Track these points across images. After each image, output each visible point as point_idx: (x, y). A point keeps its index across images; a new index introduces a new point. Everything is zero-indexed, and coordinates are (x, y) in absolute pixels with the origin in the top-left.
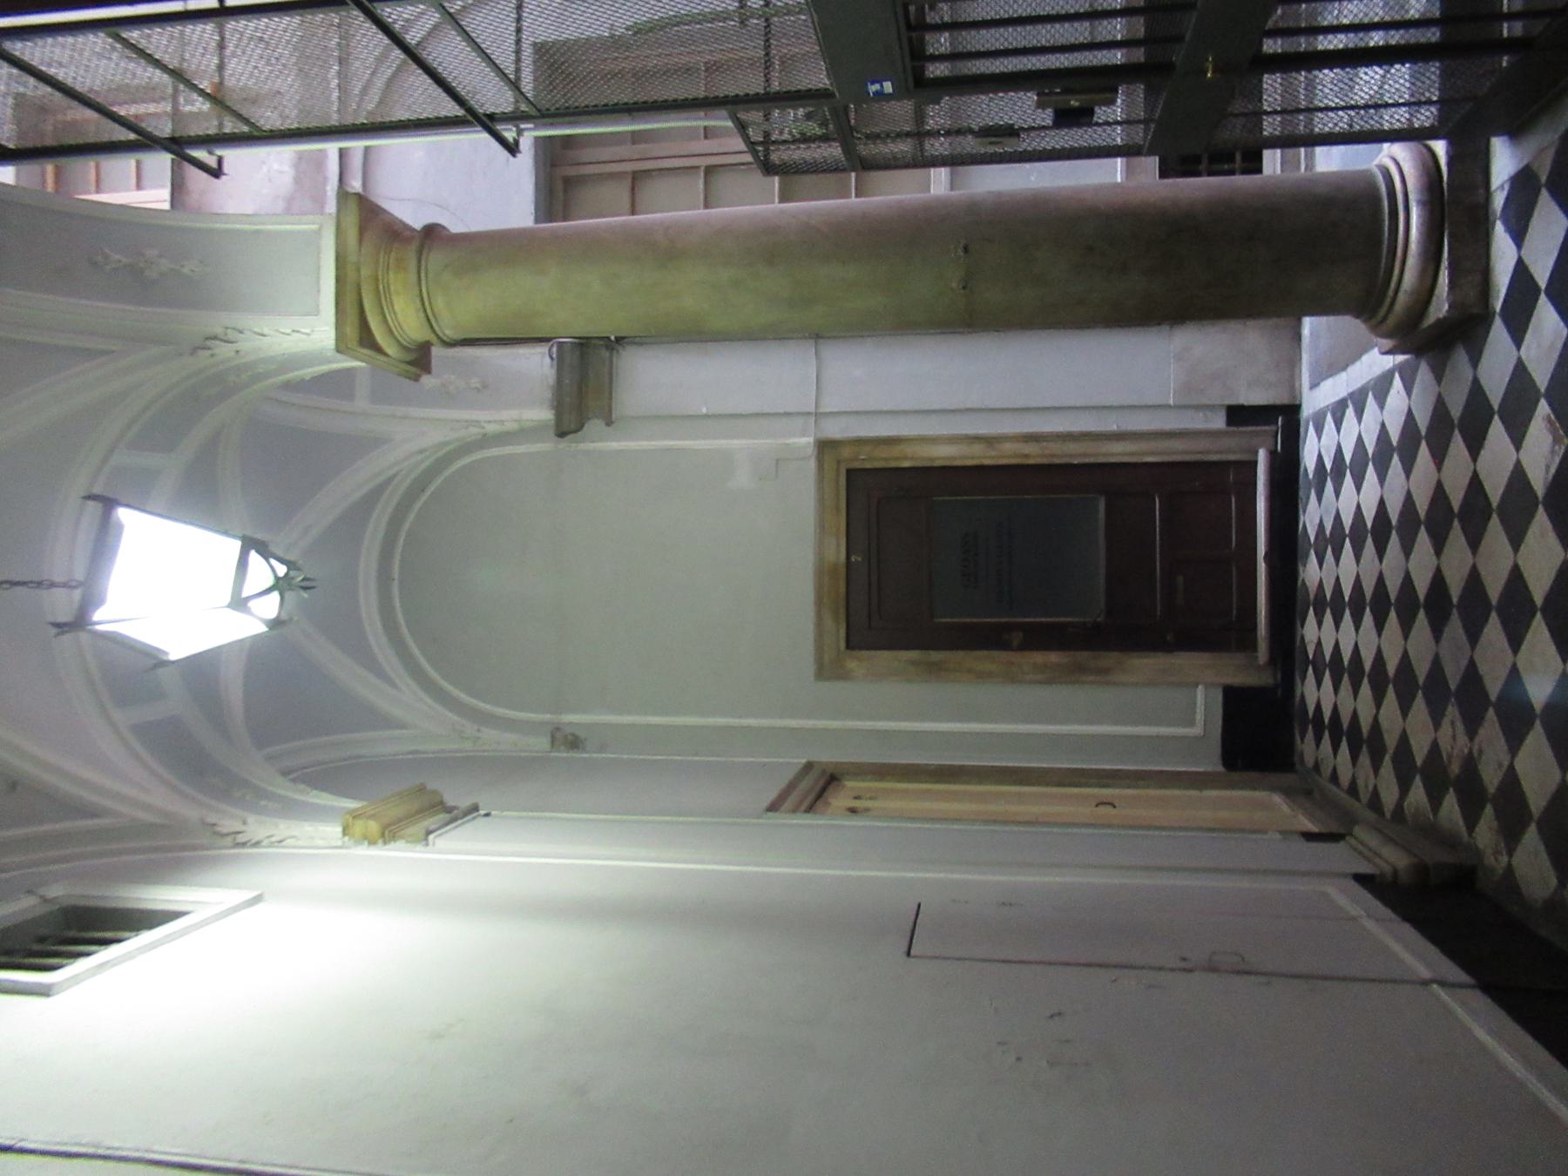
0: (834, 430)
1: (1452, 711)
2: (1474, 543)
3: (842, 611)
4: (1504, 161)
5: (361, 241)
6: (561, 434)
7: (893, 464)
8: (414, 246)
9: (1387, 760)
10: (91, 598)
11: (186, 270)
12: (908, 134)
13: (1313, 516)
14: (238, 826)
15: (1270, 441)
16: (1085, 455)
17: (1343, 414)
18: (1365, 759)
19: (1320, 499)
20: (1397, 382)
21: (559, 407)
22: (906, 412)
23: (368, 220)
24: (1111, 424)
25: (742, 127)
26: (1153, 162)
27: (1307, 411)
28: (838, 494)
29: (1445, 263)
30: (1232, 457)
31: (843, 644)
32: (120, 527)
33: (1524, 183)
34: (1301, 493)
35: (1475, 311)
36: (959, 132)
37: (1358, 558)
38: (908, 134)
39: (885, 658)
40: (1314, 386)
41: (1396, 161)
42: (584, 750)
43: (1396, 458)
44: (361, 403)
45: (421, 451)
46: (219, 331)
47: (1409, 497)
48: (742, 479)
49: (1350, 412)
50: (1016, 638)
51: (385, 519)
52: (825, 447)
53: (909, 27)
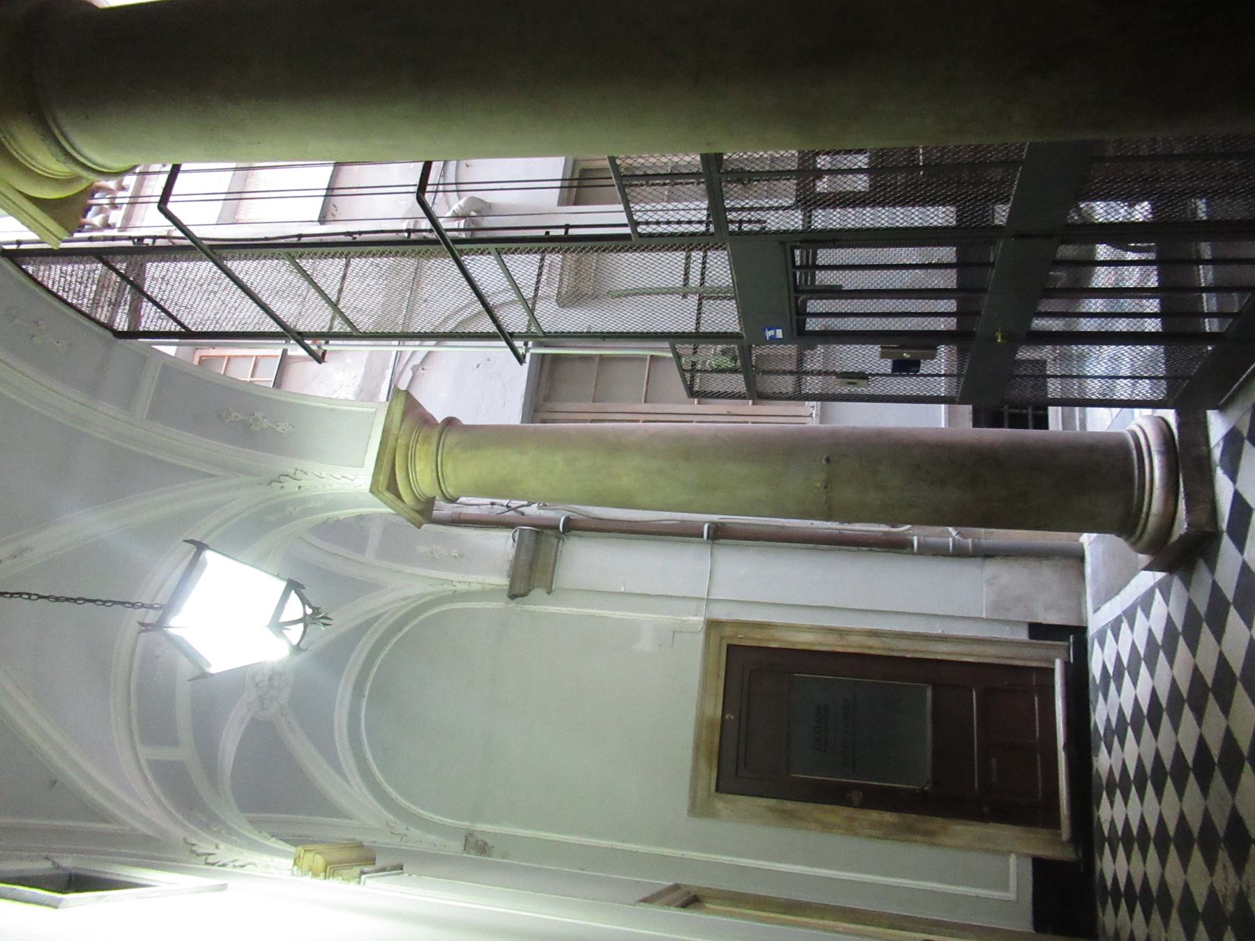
0: (721, 613)
1: (1223, 856)
2: (1226, 708)
3: (715, 762)
4: (1217, 426)
5: (402, 422)
6: (513, 597)
7: (763, 644)
8: (437, 429)
9: (1175, 915)
10: (167, 609)
11: (279, 429)
12: (791, 373)
13: (1102, 714)
14: (211, 849)
15: (1064, 653)
16: (915, 651)
17: (1119, 629)
18: (1156, 917)
19: (1106, 698)
20: (1158, 596)
21: (513, 577)
22: (779, 605)
23: (409, 409)
24: (937, 629)
25: (678, 357)
26: (966, 410)
27: (1092, 631)
28: (720, 655)
29: (1182, 495)
30: (1034, 664)
31: (713, 788)
32: (205, 564)
33: (1233, 441)
34: (1092, 697)
35: (1208, 529)
36: (827, 373)
37: (1138, 740)
38: (791, 373)
39: (746, 803)
40: (1096, 611)
41: (1141, 425)
42: (490, 856)
43: (1161, 654)
44: (369, 556)
45: (404, 599)
46: (291, 471)
47: (1174, 682)
48: (645, 644)
49: (1125, 626)
50: (857, 796)
51: (369, 646)
52: (712, 625)
53: (798, 313)
